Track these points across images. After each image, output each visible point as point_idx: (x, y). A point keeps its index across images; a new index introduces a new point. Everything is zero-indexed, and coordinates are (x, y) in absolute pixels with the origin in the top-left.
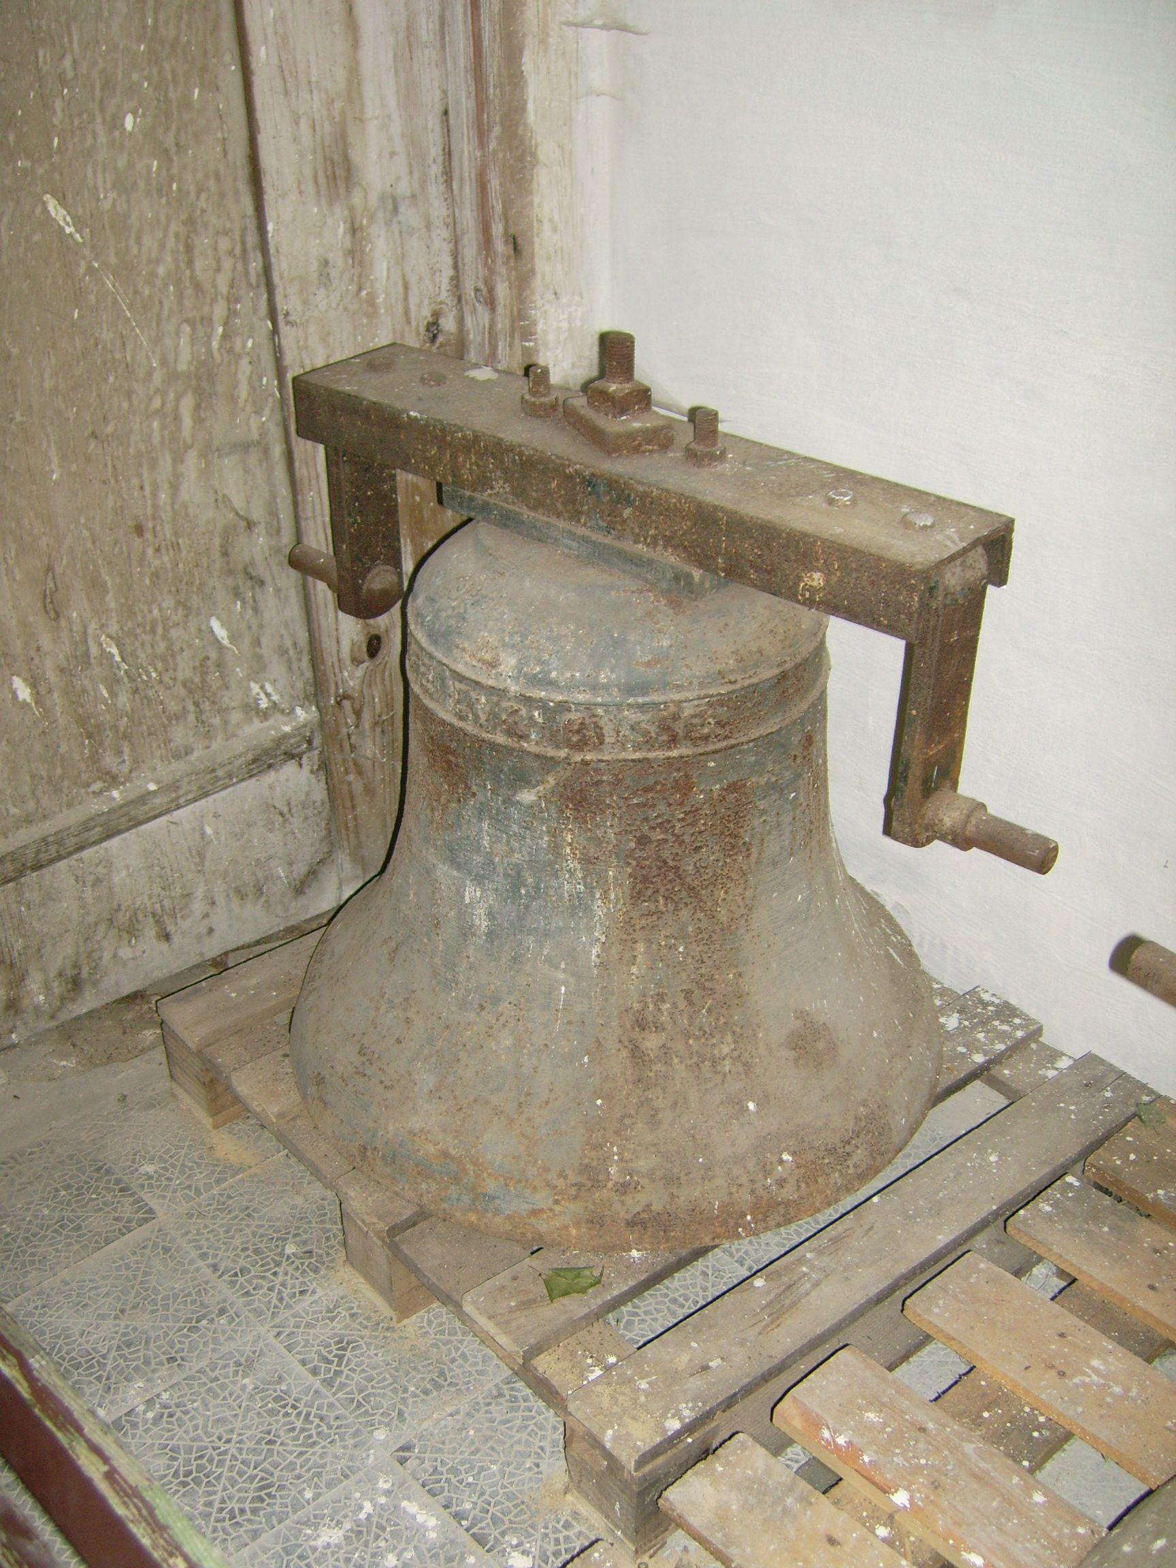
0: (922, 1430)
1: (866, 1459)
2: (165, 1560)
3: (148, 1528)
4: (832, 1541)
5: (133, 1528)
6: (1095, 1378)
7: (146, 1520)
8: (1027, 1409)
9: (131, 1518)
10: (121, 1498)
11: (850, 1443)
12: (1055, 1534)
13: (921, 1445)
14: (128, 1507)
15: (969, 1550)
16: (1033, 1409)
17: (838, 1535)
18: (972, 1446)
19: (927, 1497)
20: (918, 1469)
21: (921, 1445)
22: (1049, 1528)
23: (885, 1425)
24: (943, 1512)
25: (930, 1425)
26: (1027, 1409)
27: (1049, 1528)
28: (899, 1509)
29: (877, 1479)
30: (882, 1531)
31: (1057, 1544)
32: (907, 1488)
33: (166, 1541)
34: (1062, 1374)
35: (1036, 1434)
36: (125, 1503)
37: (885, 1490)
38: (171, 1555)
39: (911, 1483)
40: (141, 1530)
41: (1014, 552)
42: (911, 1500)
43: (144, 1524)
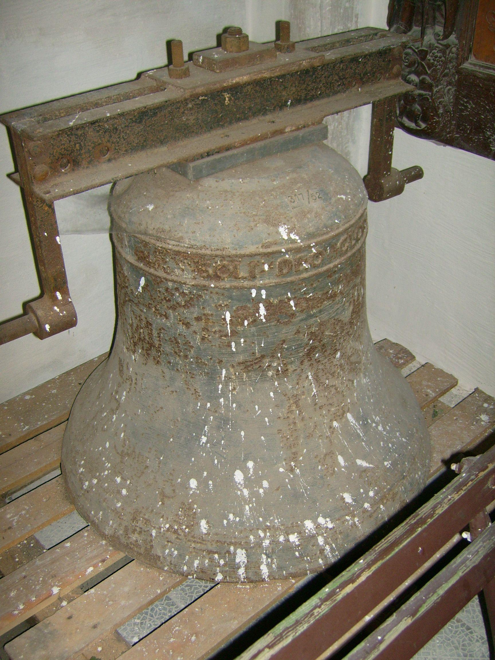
0: (25, 577)
1: (34, 599)
2: (315, 617)
3: (300, 626)
4: (70, 618)
5: (299, 633)
6: (15, 518)
7: (295, 627)
8: (19, 546)
9: (294, 633)
10: (283, 639)
11: (24, 604)
12: (86, 542)
13: (33, 578)
14: (289, 636)
15: (86, 571)
16: (19, 544)
17: (67, 615)
18: (38, 562)
19: (59, 580)
20: (44, 581)
21: (33, 578)
22: (83, 543)
23: (18, 590)
24: (67, 576)
25: (24, 574)
26: (19, 546)
27: (83, 543)
28: (59, 593)
29: (44, 597)
30: (64, 603)
31: (90, 543)
32: (52, 587)
33: (306, 618)
34: (10, 528)
35: (32, 545)
36: (286, 637)
37: (50, 595)
38: (313, 614)
39: (50, 585)
40: (301, 628)
41: (386, 20)
42: (58, 586)
43: (298, 628)
